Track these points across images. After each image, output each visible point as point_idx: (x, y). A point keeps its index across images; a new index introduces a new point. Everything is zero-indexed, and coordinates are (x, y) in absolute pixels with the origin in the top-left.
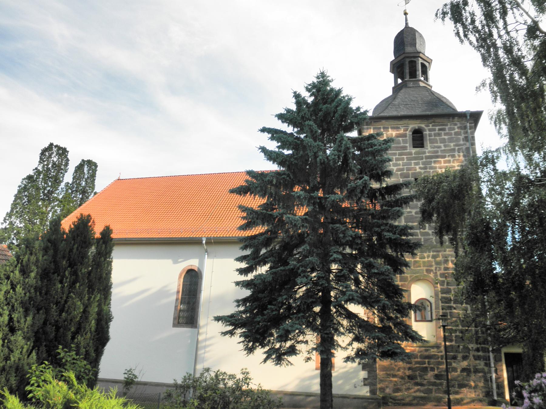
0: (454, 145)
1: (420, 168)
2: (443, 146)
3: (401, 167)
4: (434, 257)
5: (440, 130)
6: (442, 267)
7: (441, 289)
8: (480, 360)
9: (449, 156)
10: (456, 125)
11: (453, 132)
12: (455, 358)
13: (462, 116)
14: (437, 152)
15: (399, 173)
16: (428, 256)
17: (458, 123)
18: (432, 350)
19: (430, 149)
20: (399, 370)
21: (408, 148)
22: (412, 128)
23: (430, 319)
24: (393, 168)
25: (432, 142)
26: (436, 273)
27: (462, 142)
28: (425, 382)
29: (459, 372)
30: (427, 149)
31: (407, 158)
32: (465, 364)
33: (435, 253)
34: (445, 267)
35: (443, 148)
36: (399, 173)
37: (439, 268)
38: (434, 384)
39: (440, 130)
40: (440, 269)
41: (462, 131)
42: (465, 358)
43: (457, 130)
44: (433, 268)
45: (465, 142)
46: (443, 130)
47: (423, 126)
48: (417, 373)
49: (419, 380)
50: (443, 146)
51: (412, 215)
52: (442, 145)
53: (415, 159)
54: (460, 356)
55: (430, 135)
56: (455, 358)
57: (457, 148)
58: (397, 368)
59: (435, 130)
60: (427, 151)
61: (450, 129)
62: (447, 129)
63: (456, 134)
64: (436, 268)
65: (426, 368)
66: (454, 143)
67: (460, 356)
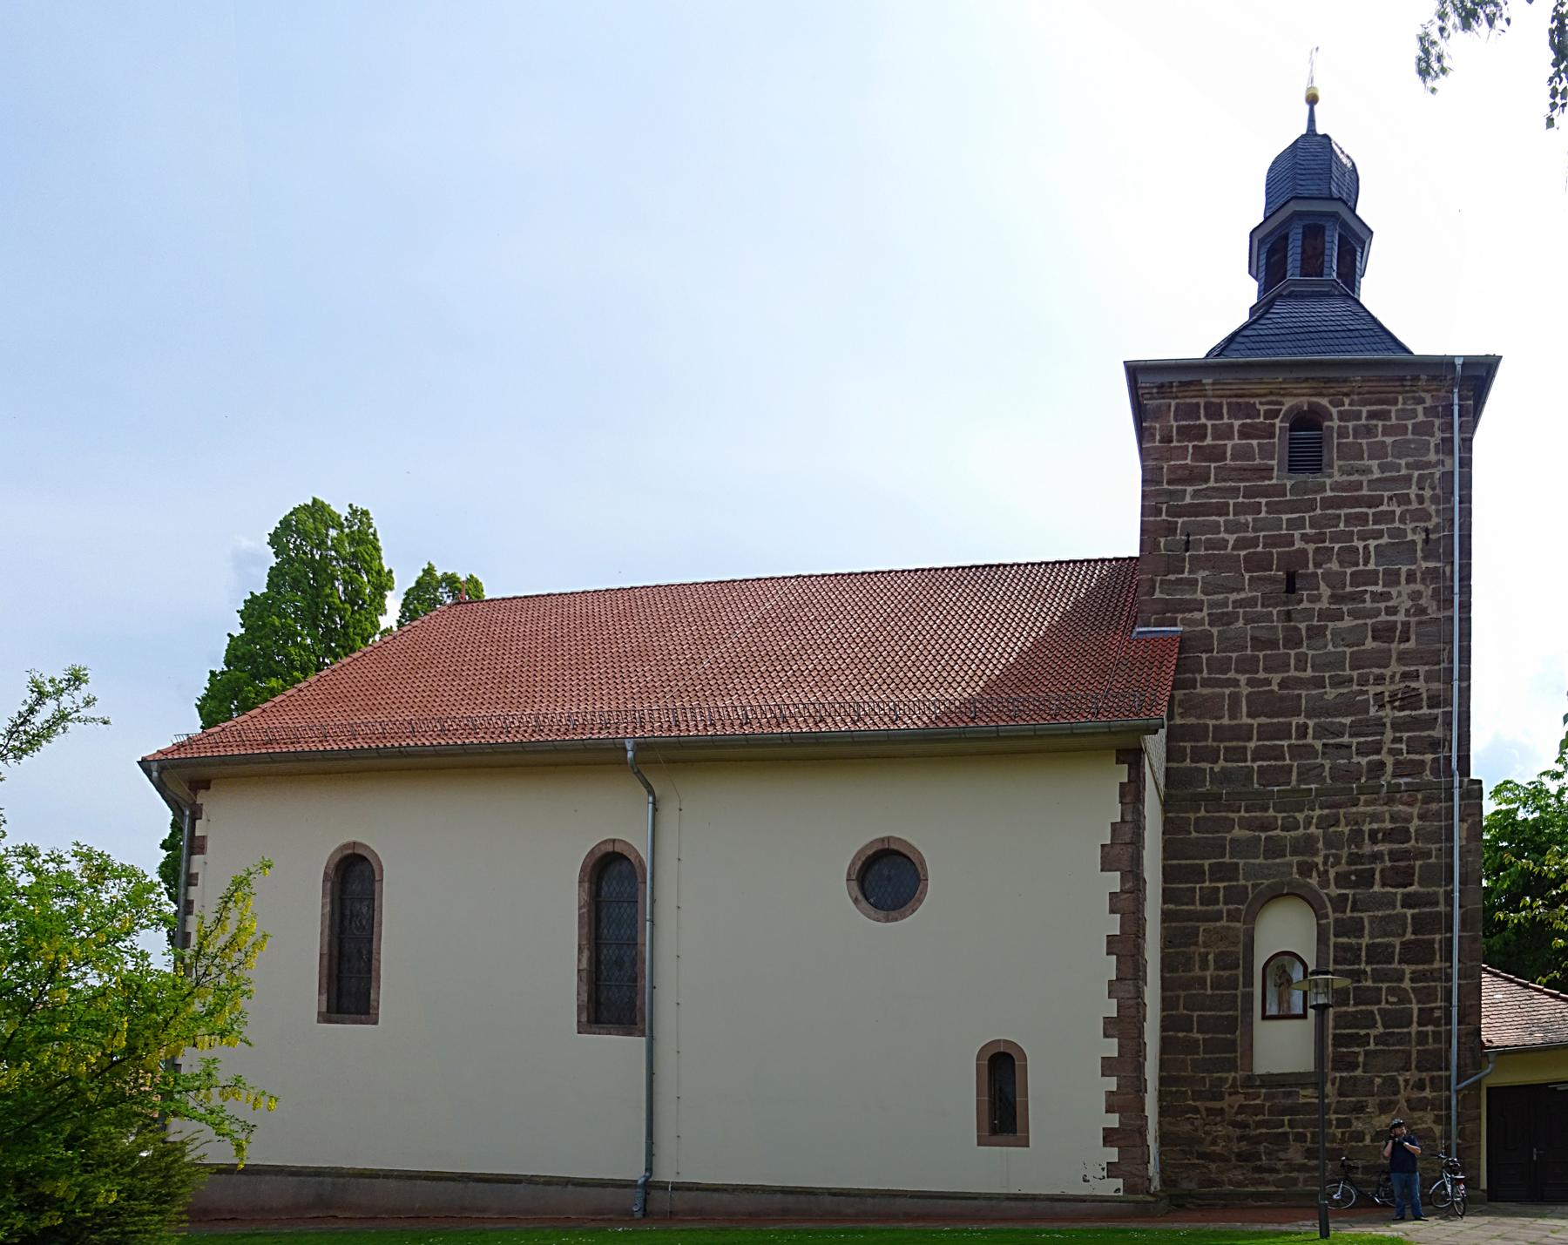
0: (1408, 466)
1: (1304, 537)
2: (1375, 469)
3: (1251, 534)
4: (1323, 823)
5: (1371, 415)
6: (1345, 853)
7: (1336, 920)
8: (1424, 1109)
9: (1390, 498)
10: (1421, 401)
11: (1410, 423)
12: (1359, 1108)
13: (1439, 367)
14: (1359, 486)
15: (1243, 553)
16: (1308, 823)
17: (1427, 397)
18: (1302, 1092)
19: (1338, 478)
20: (1214, 1143)
21: (1275, 473)
22: (1291, 409)
23: (1299, 1011)
24: (1226, 536)
25: (1346, 453)
26: (1326, 872)
27: (1432, 457)
28: (1280, 1165)
29: (1368, 1141)
30: (1330, 476)
31: (1267, 504)
32: (1383, 1121)
33: (1326, 811)
34: (1351, 854)
35: (1377, 475)
36: (1243, 553)
37: (1335, 856)
38: (1302, 1168)
39: (1371, 415)
40: (1337, 862)
41: (1437, 422)
42: (1384, 1108)
43: (1421, 418)
44: (1319, 860)
45: (1441, 457)
46: (1384, 415)
47: (1324, 402)
48: (1262, 1148)
49: (1264, 1161)
50: (1375, 469)
51: (1272, 691)
52: (1374, 463)
53: (1293, 507)
54: (1372, 1103)
55: (1342, 433)
56: (1359, 1108)
57: (1416, 474)
58: (1209, 1139)
59: (1358, 416)
60: (1328, 481)
61: (1404, 415)
62: (1393, 415)
63: (1417, 429)
64: (1326, 857)
65: (1286, 1134)
66: (1411, 460)
67: (1372, 1103)
